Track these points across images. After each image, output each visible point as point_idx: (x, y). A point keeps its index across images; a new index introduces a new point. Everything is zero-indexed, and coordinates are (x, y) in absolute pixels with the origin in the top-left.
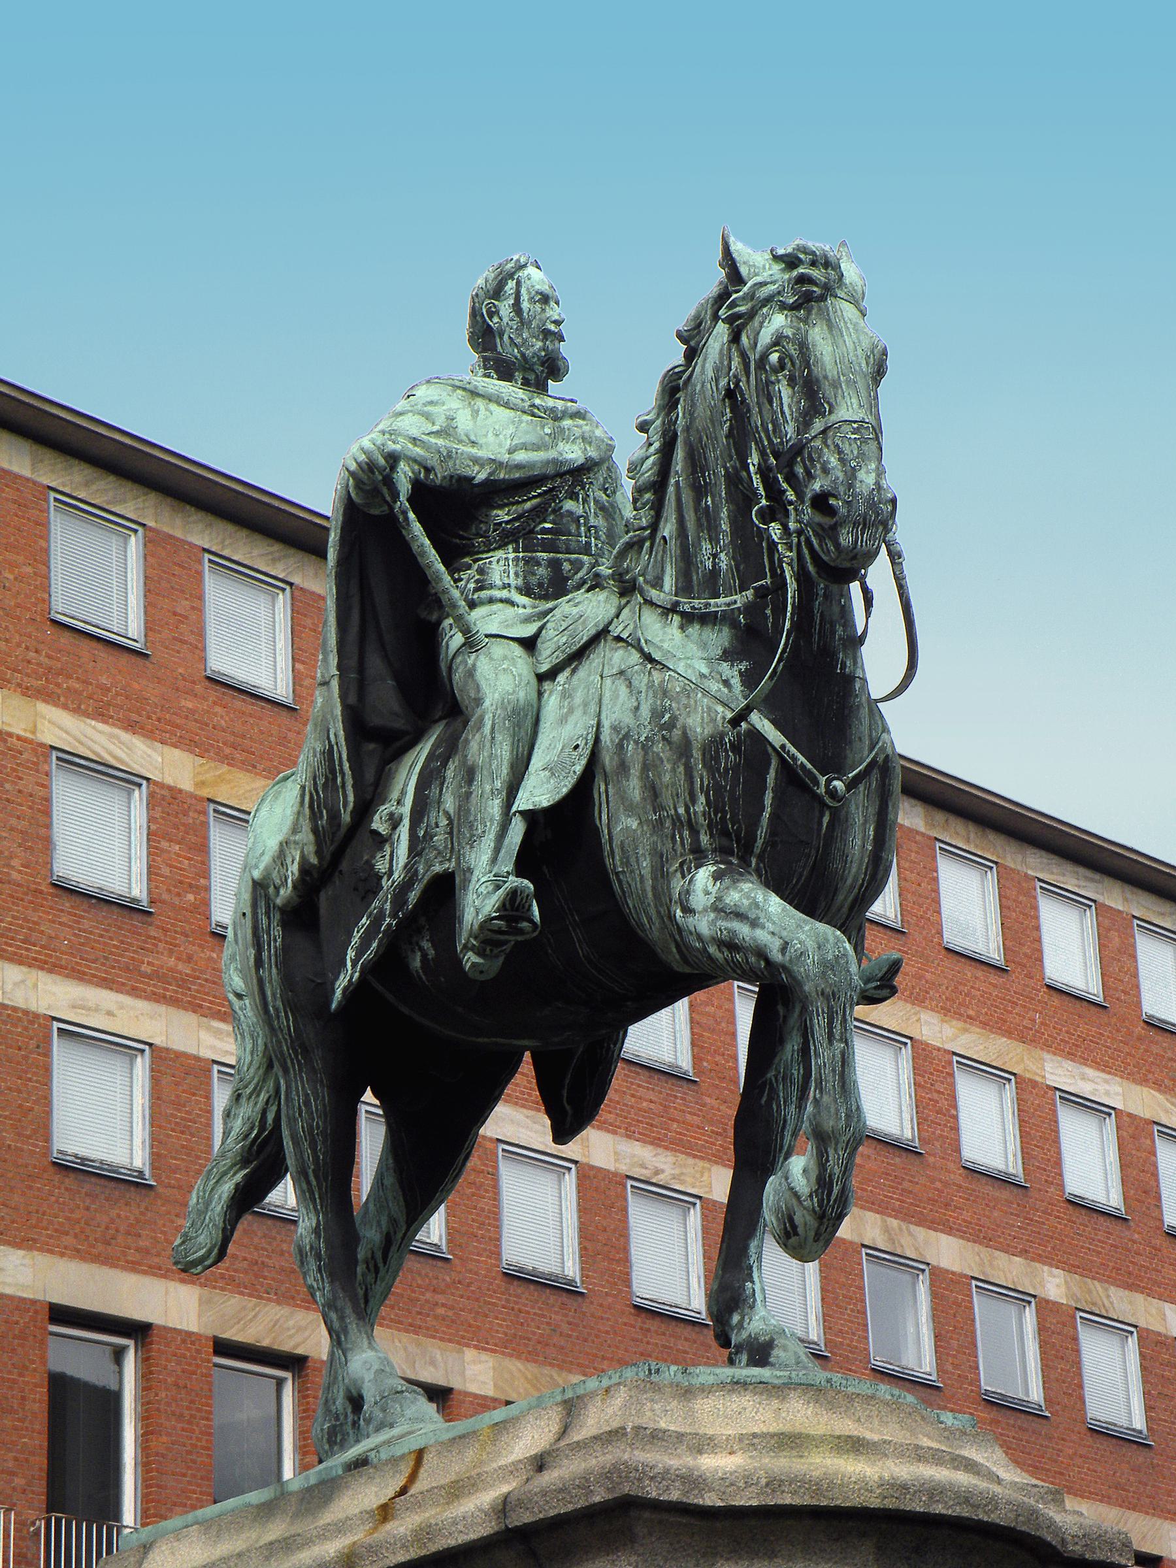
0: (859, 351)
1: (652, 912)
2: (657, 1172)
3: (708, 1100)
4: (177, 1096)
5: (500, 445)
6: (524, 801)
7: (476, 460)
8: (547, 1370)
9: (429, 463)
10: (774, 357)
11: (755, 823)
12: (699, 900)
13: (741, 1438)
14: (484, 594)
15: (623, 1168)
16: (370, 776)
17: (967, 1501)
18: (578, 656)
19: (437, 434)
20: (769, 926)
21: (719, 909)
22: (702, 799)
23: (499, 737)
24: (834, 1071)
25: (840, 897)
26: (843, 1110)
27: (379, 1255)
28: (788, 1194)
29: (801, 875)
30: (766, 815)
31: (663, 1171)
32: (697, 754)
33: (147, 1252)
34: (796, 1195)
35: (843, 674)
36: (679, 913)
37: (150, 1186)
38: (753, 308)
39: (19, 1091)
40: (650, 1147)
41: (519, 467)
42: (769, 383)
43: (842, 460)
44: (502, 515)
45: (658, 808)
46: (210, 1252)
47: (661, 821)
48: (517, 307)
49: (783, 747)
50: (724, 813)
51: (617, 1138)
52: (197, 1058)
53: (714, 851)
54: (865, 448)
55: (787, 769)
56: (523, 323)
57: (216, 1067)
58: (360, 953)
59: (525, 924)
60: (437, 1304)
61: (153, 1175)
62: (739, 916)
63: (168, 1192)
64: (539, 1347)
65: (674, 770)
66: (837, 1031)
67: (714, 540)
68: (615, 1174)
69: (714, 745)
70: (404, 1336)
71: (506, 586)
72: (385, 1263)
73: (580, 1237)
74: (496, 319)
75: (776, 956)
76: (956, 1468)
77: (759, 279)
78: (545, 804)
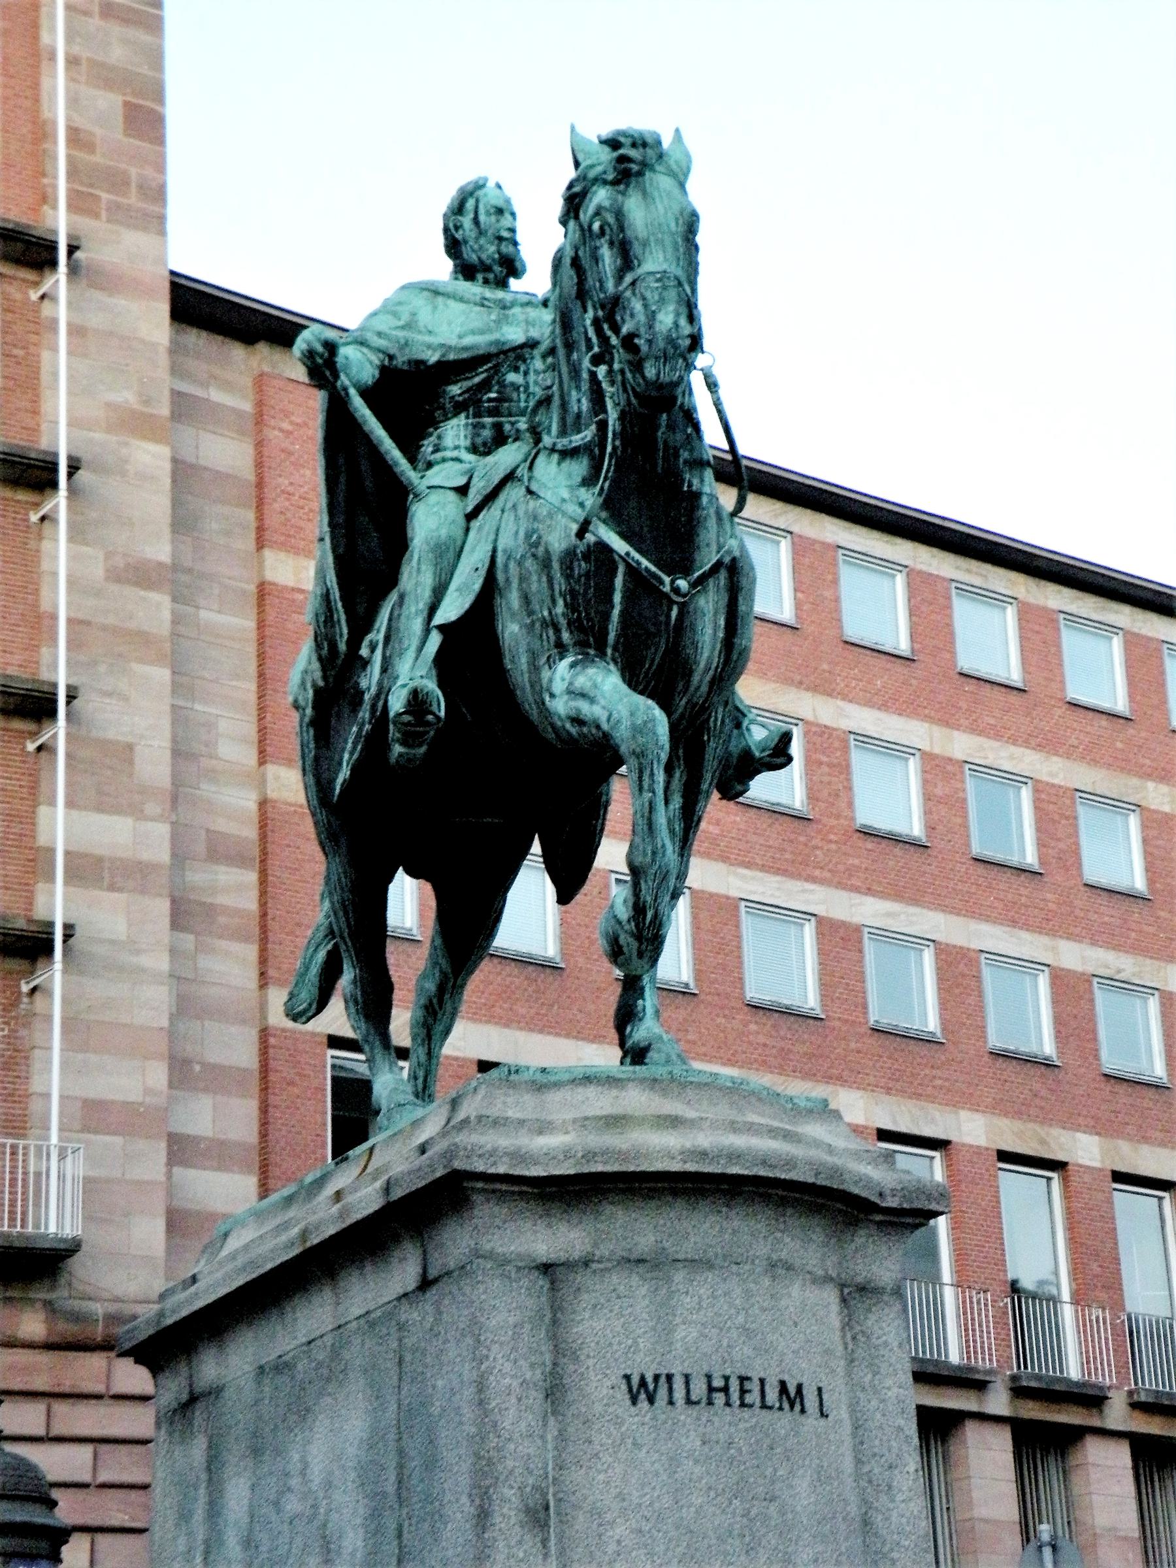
0: (669, 214)
1: (531, 699)
2: (1119, 972)
3: (1162, 914)
4: (713, 926)
5: (452, 332)
6: (440, 618)
7: (429, 347)
8: (1030, 1125)
9: (392, 352)
10: (596, 226)
11: (606, 616)
12: (558, 687)
13: (575, 1121)
14: (438, 456)
15: (1091, 970)
16: (361, 609)
17: (764, 1163)
18: (491, 497)
19: (403, 328)
20: (603, 702)
21: (571, 692)
22: (561, 602)
23: (423, 567)
24: (643, 816)
25: (696, 678)
26: (650, 848)
27: (435, 1001)
28: (613, 922)
29: (653, 660)
30: (616, 612)
31: (1124, 970)
32: (556, 565)
33: (694, 1043)
34: (619, 922)
35: (690, 492)
36: (547, 698)
37: (694, 994)
38: (584, 188)
39: (587, 926)
40: (1113, 952)
41: (465, 349)
42: (596, 248)
43: (646, 306)
44: (455, 390)
45: (530, 613)
46: (310, 1005)
47: (533, 623)
48: (476, 221)
49: (628, 554)
50: (580, 613)
51: (1083, 946)
52: (728, 898)
53: (575, 644)
54: (665, 294)
55: (633, 572)
56: (481, 233)
57: (743, 903)
58: (352, 753)
59: (430, 717)
60: (934, 1077)
61: (697, 986)
62: (583, 695)
63: (709, 998)
64: (1023, 1108)
65: (539, 581)
66: (646, 786)
67: (578, 388)
68: (1083, 974)
69: (569, 555)
70: (911, 1103)
71: (457, 448)
72: (441, 1008)
73: (1055, 1023)
74: (461, 232)
75: (605, 726)
76: (774, 1138)
77: (589, 162)
78: (453, 618)
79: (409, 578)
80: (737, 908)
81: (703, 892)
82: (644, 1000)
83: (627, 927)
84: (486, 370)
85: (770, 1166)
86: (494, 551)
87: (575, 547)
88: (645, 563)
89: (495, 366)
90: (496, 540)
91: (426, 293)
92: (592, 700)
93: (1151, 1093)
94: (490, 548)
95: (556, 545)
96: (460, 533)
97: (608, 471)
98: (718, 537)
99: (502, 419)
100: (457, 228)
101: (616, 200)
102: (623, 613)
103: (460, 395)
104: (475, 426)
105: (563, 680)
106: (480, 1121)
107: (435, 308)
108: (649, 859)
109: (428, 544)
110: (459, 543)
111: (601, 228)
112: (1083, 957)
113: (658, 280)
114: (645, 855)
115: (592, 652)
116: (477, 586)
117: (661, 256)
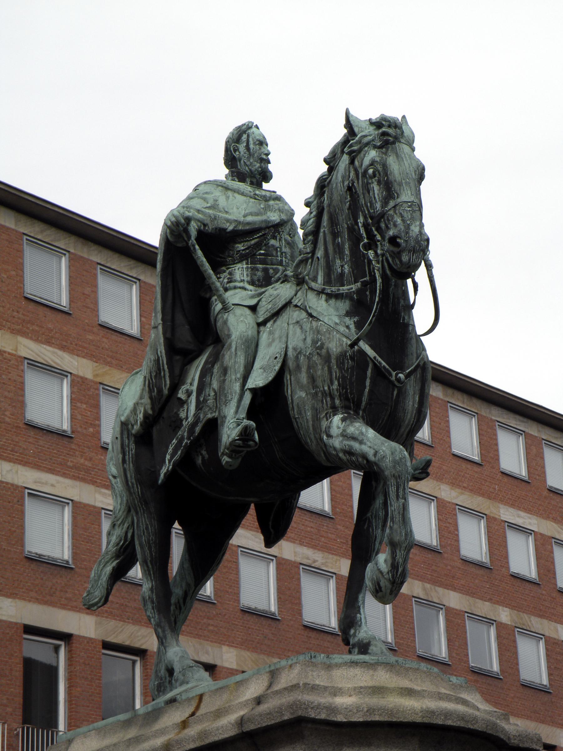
0: (411, 168)
3: (339, 527)
5: (239, 213)
6: (251, 384)
7: (228, 221)
8: (262, 656)
9: (206, 222)
10: (371, 171)
12: (335, 431)
13: (355, 688)
14: (232, 285)
15: (298, 560)
17: (463, 719)
18: (277, 314)
19: (209, 208)
20: (368, 443)
21: (344, 435)
22: (336, 383)
23: (239, 353)
24: (399, 513)
27: (181, 601)
28: (377, 572)
30: (367, 390)
31: (317, 561)
32: (334, 361)
34: (381, 572)
35: (404, 323)
36: (325, 437)
39: (9, 523)
40: (311, 550)
41: (248, 223)
43: (403, 221)
44: (240, 247)
45: (315, 387)
46: (100, 599)
47: (316, 393)
48: (247, 147)
49: (375, 358)
50: (347, 389)
51: (295, 545)
52: (94, 507)
53: (342, 407)
54: (414, 215)
55: (377, 368)
57: (103, 511)
58: (172, 456)
60: (209, 625)
61: (73, 563)
62: (354, 438)
65: (323, 369)
66: (401, 494)
67: (342, 259)
68: (295, 562)
69: (342, 357)
71: (242, 281)
72: (184, 605)
74: (237, 153)
76: (458, 703)
79: (230, 358)
80: (100, 513)
81: (80, 503)
82: (360, 614)
83: (386, 576)
84: (258, 237)
85: (466, 721)
86: (287, 347)
87: (346, 352)
88: (384, 363)
89: (264, 235)
90: (287, 342)
91: (220, 188)
92: (361, 442)
93: (329, 638)
94: (284, 346)
95: (334, 350)
96: (256, 333)
97: (375, 312)
98: (417, 350)
99: (268, 266)
100: (235, 151)
101: (382, 158)
102: (371, 391)
103: (243, 250)
104: (252, 269)
105: (339, 428)
106: (305, 687)
107: (228, 198)
108: (403, 538)
109: (241, 339)
110: (256, 338)
111: (374, 172)
112: (295, 552)
113: (409, 207)
114: (401, 536)
115: (352, 413)
116: (277, 368)
117: (409, 192)
